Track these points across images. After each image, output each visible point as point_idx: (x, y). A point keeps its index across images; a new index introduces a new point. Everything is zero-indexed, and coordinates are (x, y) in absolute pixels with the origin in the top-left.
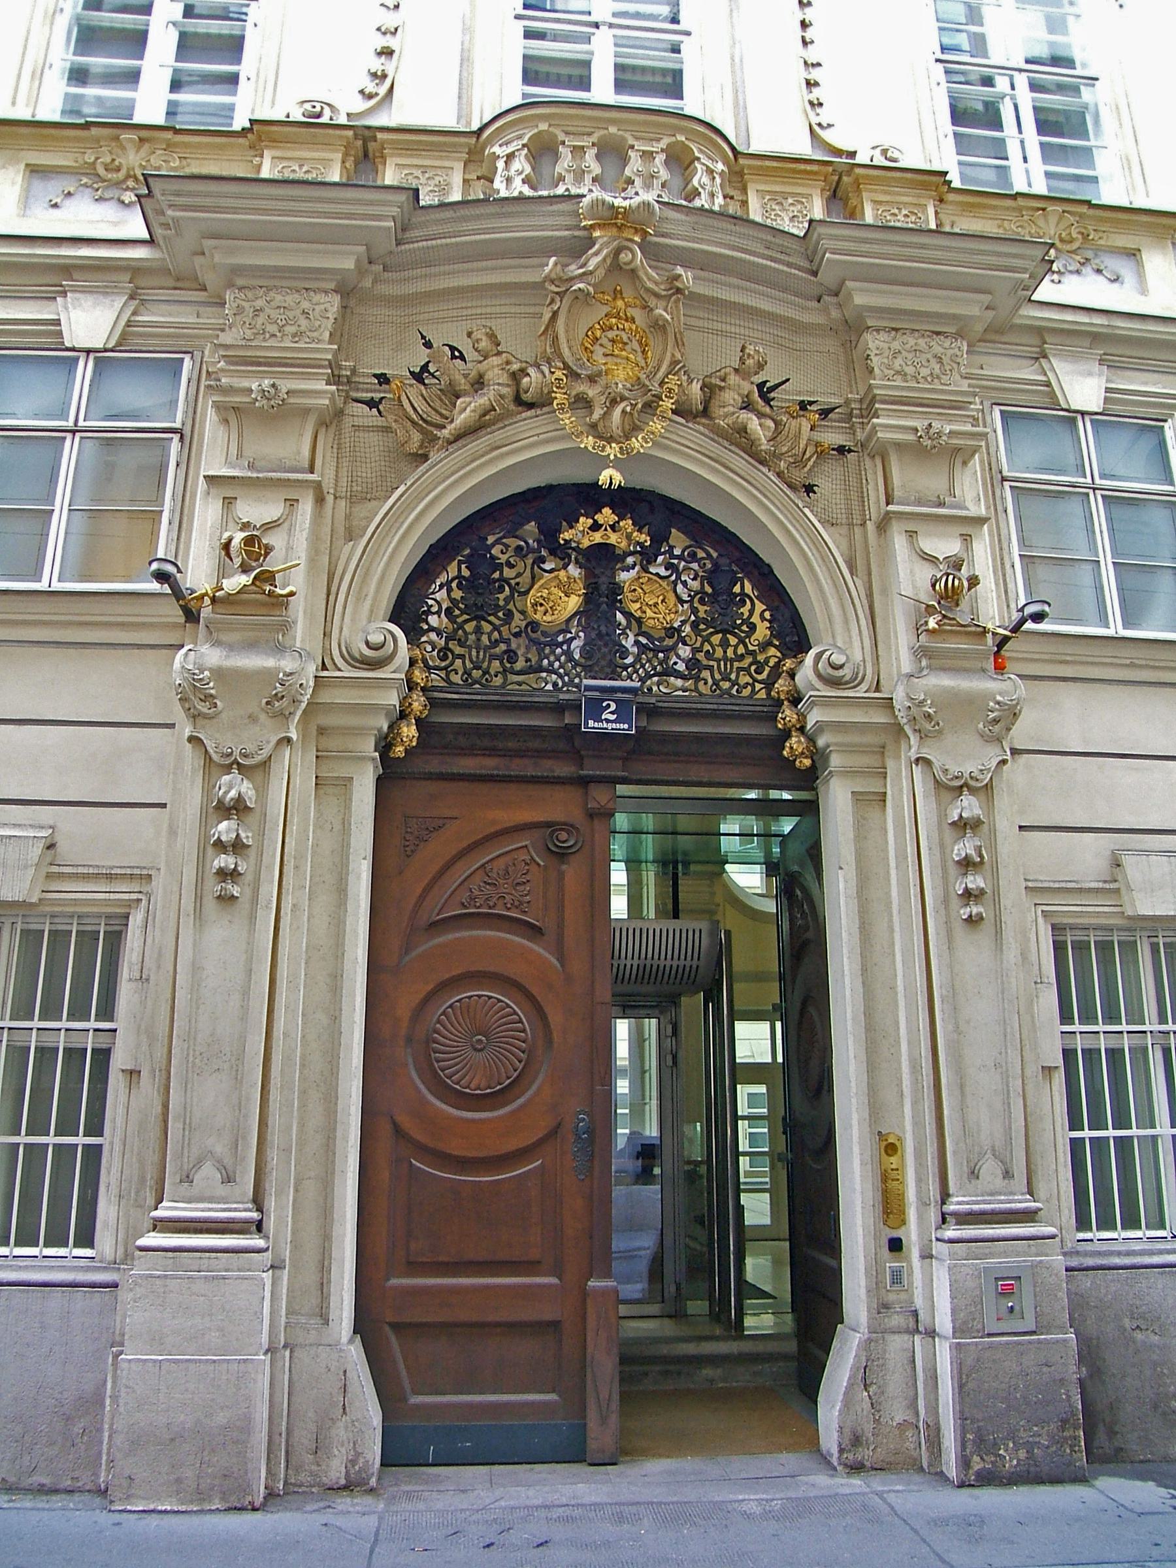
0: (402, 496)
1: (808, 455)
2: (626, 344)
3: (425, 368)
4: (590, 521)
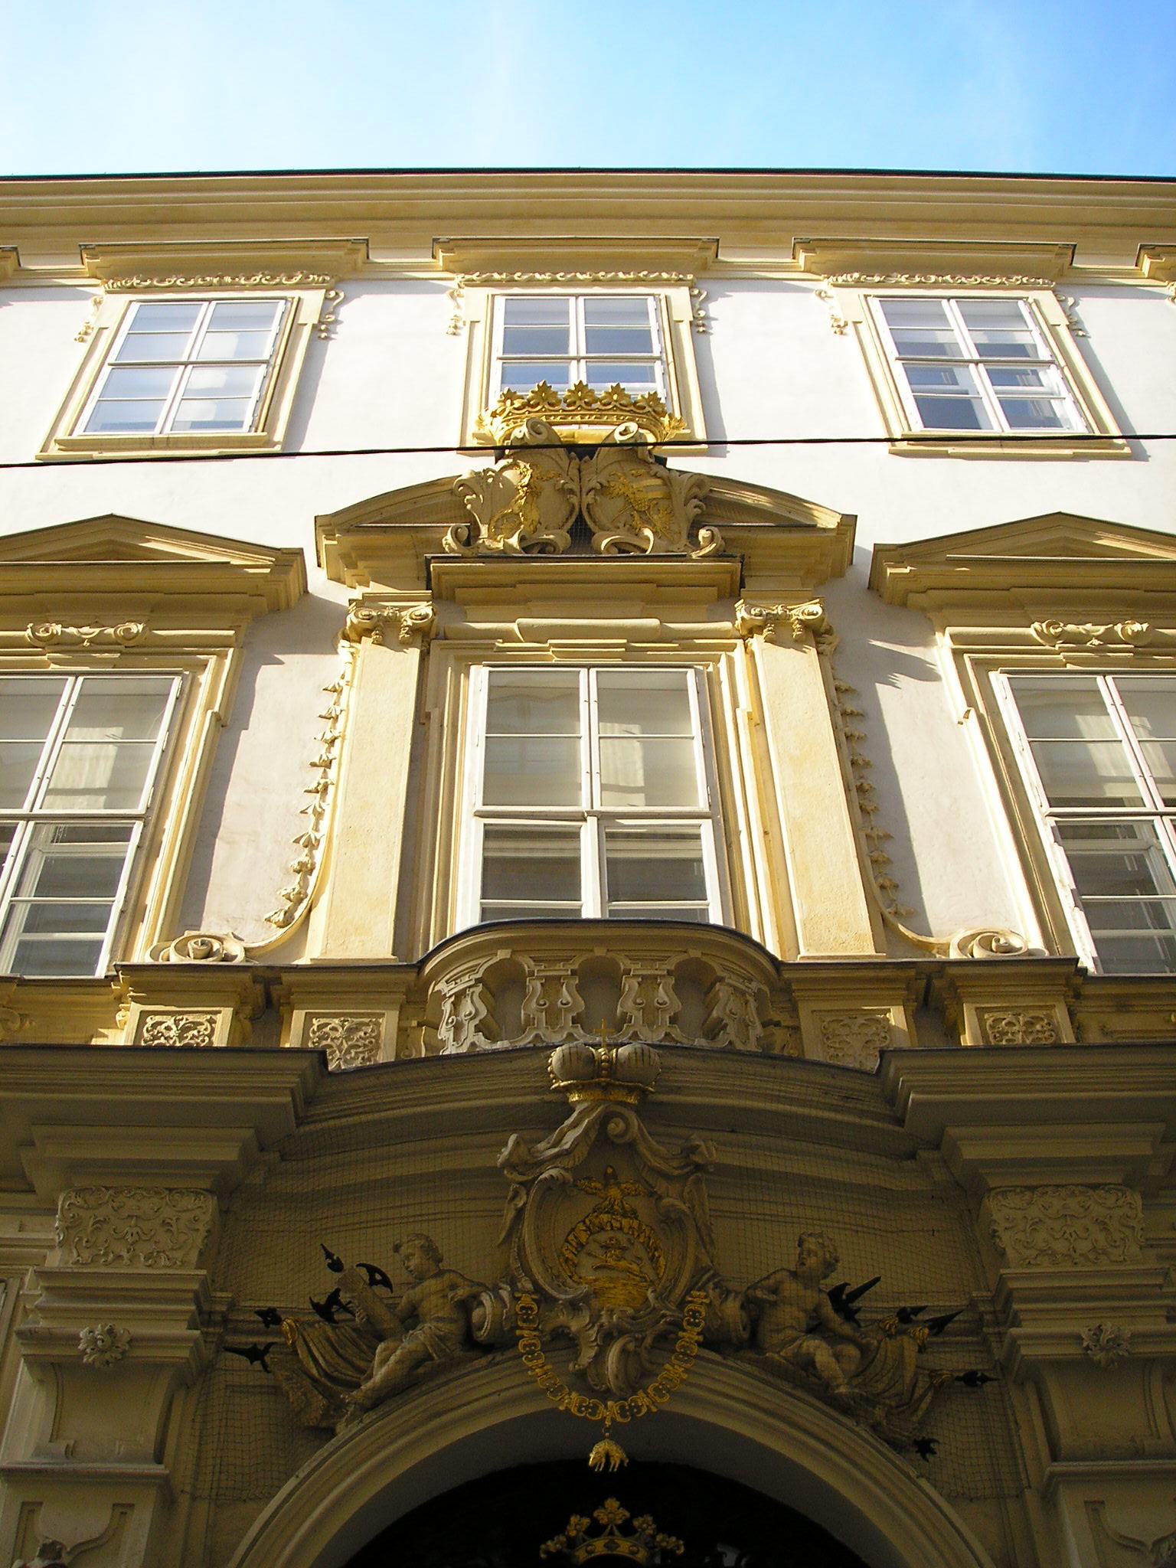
0: (290, 1495)
1: (919, 1391)
2: (624, 1249)
3: (334, 1298)
4: (586, 1521)
